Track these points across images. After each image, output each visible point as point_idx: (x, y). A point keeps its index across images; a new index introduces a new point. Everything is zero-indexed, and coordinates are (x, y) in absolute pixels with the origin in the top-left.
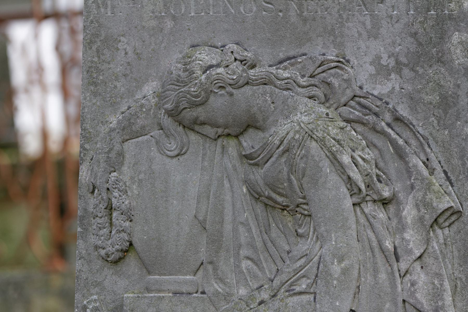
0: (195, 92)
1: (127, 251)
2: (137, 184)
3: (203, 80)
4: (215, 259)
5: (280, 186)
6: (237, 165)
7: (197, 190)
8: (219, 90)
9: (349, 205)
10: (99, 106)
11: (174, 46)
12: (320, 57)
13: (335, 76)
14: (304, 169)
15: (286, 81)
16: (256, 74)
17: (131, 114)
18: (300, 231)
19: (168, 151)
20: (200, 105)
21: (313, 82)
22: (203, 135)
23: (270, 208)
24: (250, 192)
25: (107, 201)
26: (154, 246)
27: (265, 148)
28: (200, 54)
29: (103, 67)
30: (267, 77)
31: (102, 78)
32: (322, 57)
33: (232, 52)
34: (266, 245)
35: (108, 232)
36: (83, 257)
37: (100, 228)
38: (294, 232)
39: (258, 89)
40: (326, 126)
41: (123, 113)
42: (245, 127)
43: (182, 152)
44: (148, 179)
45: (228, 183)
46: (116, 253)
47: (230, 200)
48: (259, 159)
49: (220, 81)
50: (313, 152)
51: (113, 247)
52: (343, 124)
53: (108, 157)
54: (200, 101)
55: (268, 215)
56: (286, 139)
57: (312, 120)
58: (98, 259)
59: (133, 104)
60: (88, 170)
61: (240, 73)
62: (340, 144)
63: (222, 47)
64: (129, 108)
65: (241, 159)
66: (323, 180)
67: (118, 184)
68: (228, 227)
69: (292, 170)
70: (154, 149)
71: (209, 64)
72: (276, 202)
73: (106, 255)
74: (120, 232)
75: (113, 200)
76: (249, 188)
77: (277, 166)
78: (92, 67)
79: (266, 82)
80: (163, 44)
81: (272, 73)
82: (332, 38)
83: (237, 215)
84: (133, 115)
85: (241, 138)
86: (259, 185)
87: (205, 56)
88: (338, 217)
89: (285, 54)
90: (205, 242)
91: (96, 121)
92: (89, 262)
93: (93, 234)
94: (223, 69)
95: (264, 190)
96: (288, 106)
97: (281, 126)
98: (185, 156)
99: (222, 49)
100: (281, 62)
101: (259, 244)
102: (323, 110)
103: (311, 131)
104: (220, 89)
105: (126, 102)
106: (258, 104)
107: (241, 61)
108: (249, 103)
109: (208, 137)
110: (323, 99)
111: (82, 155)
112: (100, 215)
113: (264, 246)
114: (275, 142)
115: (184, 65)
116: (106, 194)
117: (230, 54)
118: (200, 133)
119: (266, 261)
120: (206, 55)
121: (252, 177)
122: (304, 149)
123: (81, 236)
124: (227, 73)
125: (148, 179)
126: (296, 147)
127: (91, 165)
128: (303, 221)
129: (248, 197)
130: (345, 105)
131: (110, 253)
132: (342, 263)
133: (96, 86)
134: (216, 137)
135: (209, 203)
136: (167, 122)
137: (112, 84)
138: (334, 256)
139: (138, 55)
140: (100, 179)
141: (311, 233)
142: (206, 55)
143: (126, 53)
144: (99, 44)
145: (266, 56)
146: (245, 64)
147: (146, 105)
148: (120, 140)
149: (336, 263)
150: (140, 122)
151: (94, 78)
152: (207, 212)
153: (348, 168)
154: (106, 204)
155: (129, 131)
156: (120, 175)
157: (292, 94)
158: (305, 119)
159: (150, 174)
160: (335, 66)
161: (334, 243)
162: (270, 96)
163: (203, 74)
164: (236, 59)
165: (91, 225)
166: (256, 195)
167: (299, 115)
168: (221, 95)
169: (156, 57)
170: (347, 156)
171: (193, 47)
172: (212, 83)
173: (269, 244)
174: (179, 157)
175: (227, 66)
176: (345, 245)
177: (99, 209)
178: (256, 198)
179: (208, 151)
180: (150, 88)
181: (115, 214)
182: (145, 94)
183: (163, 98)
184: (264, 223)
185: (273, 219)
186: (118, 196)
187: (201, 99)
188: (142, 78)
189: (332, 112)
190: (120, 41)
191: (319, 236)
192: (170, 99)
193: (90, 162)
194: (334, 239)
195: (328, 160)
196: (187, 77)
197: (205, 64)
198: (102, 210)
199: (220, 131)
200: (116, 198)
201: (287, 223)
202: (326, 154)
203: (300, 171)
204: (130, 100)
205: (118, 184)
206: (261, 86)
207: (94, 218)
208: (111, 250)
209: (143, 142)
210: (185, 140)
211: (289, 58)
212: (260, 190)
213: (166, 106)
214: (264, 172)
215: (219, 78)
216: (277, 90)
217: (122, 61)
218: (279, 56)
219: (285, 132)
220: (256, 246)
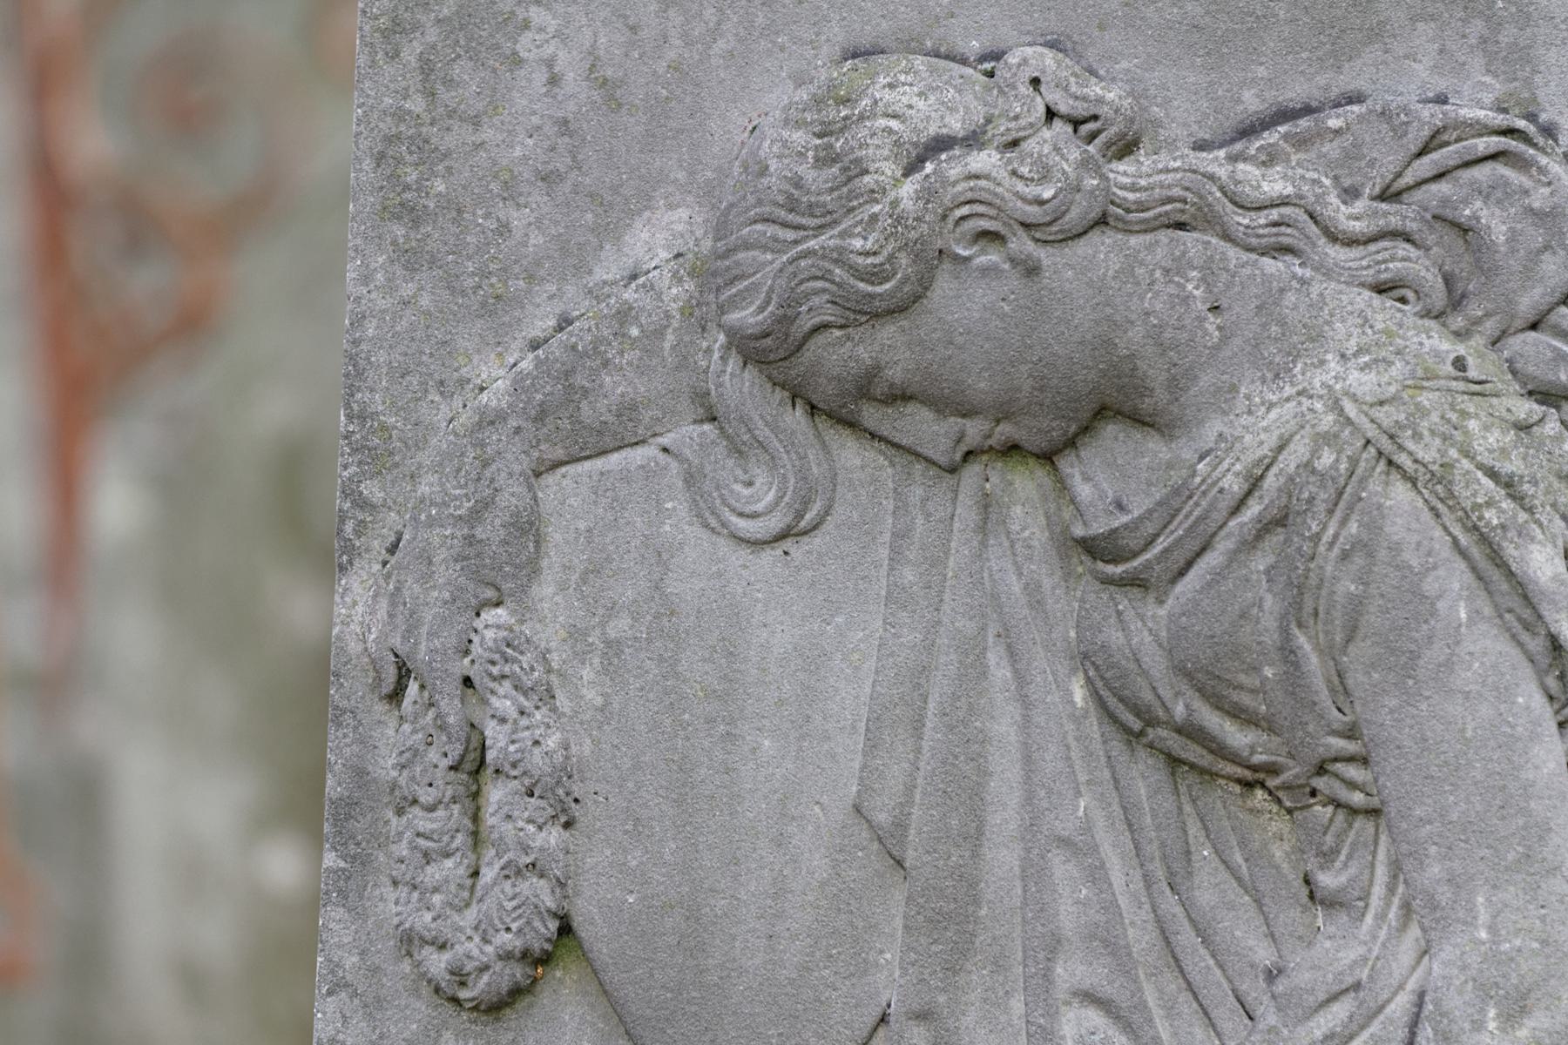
0: (867, 254)
1: (545, 960)
2: (596, 661)
3: (907, 204)
4: (942, 999)
5: (1242, 678)
6: (1047, 583)
7: (868, 690)
8: (976, 248)
9: (1552, 765)
10: (428, 314)
11: (769, 53)
12: (1426, 112)
13: (1493, 193)
14: (1356, 606)
15: (1274, 214)
16: (1143, 182)
17: (574, 348)
18: (1328, 880)
19: (741, 515)
20: (890, 312)
21: (1394, 222)
22: (897, 446)
23: (1193, 778)
24: (1101, 703)
25: (463, 735)
26: (673, 940)
27: (1178, 510)
28: (891, 86)
29: (450, 141)
30: (1189, 196)
31: (442, 188)
32: (1437, 108)
33: (1035, 82)
34: (1172, 938)
35: (461, 871)
36: (347, 985)
37: (426, 854)
38: (1298, 882)
39: (1150, 248)
40: (1453, 416)
41: (535, 345)
42: (1086, 415)
43: (803, 524)
44: (649, 640)
45: (1004, 663)
46: (498, 966)
47: (1013, 738)
48: (1148, 556)
49: (980, 209)
50: (1396, 529)
51: (486, 941)
52: (1526, 409)
53: (470, 540)
54: (891, 294)
55: (1180, 809)
56: (1274, 470)
57: (1392, 389)
58: (416, 992)
59: (579, 306)
60: (376, 596)
61: (1072, 176)
62: (1518, 498)
63: (983, 58)
64: (564, 322)
65: (1064, 557)
66: (1436, 653)
67: (515, 661)
68: (1002, 860)
69: (1297, 612)
70: (677, 504)
71: (933, 130)
72: (1220, 750)
73: (452, 973)
74: (519, 873)
75: (491, 729)
76: (1099, 684)
77: (1230, 592)
78: (398, 137)
79: (1183, 218)
80: (721, 44)
81: (1212, 177)
82: (1478, 27)
83: (1045, 804)
84: (585, 354)
85: (1066, 464)
86: (1145, 673)
87: (915, 99)
88: (1503, 818)
89: (1270, 95)
90: (899, 922)
91: (414, 381)
92: (374, 1006)
93: (395, 883)
94: (996, 156)
95: (1166, 693)
96: (1282, 323)
97: (1250, 412)
98: (817, 541)
99: (988, 66)
100: (1248, 131)
101: (1140, 937)
102: (1438, 343)
103: (1392, 437)
104: (983, 242)
105: (551, 297)
106: (1147, 314)
107: (1076, 123)
108: (1109, 310)
109: (918, 455)
110: (1439, 298)
111: (349, 527)
112: (427, 796)
113: (1160, 944)
114: (1225, 483)
115: (820, 136)
116: (457, 701)
117: (1025, 90)
118: (881, 439)
119: (1170, 1011)
120: (920, 94)
121: (1115, 637)
122: (1355, 517)
123: (340, 892)
124: (1014, 173)
125: (649, 640)
126: (1321, 507)
127: (388, 576)
128: (1340, 837)
129: (1094, 727)
130: (1534, 326)
131: (469, 967)
132: (1521, 1025)
133: (416, 223)
134: (958, 456)
135: (918, 751)
136: (739, 386)
137: (487, 216)
138: (1485, 991)
139: (609, 91)
140: (432, 634)
141: (1378, 890)
142: (920, 94)
143: (554, 80)
144: (432, 35)
145: (1183, 103)
146: (1092, 137)
147: (642, 309)
148: (525, 464)
149: (1492, 1025)
150: (615, 387)
151: (407, 188)
152: (910, 789)
153: (1554, 602)
154: (456, 750)
155: (569, 424)
156: (522, 622)
157: (1299, 271)
158: (1363, 382)
159: (657, 616)
160: (1492, 150)
161: (1483, 935)
162: (1203, 279)
163: (906, 175)
164: (1051, 114)
165: (383, 842)
166: (1129, 719)
167: (1333, 364)
168: (985, 271)
169: (688, 99)
170: (1549, 549)
171: (855, 56)
172: (944, 217)
173: (1186, 938)
174: (787, 544)
175: (1015, 143)
176: (1536, 945)
177: (425, 771)
178: (1127, 730)
179: (920, 521)
180: (660, 238)
181: (496, 794)
182: (637, 263)
183: (720, 281)
184: (1163, 845)
185: (1206, 829)
186: (515, 715)
187: (898, 288)
188: (625, 191)
189: (1481, 356)
190: (526, 25)
191: (1416, 904)
192: (754, 288)
193: (385, 563)
194: (1483, 917)
195: (1461, 565)
196: (832, 190)
197: (915, 130)
198: (439, 773)
199: (974, 430)
200: (503, 721)
201: (1265, 845)
202: (1455, 541)
203: (1337, 614)
204: (570, 290)
205: (515, 661)
206: (1164, 236)
207: (400, 812)
208: (475, 953)
209: (626, 477)
210: (815, 470)
211: (1285, 115)
212: (1147, 696)
213: (734, 317)
214: (1170, 615)
215: (976, 196)
216: (1232, 253)
217: (534, 113)
218: (1239, 101)
219: (1272, 440)
220: (1127, 946)
